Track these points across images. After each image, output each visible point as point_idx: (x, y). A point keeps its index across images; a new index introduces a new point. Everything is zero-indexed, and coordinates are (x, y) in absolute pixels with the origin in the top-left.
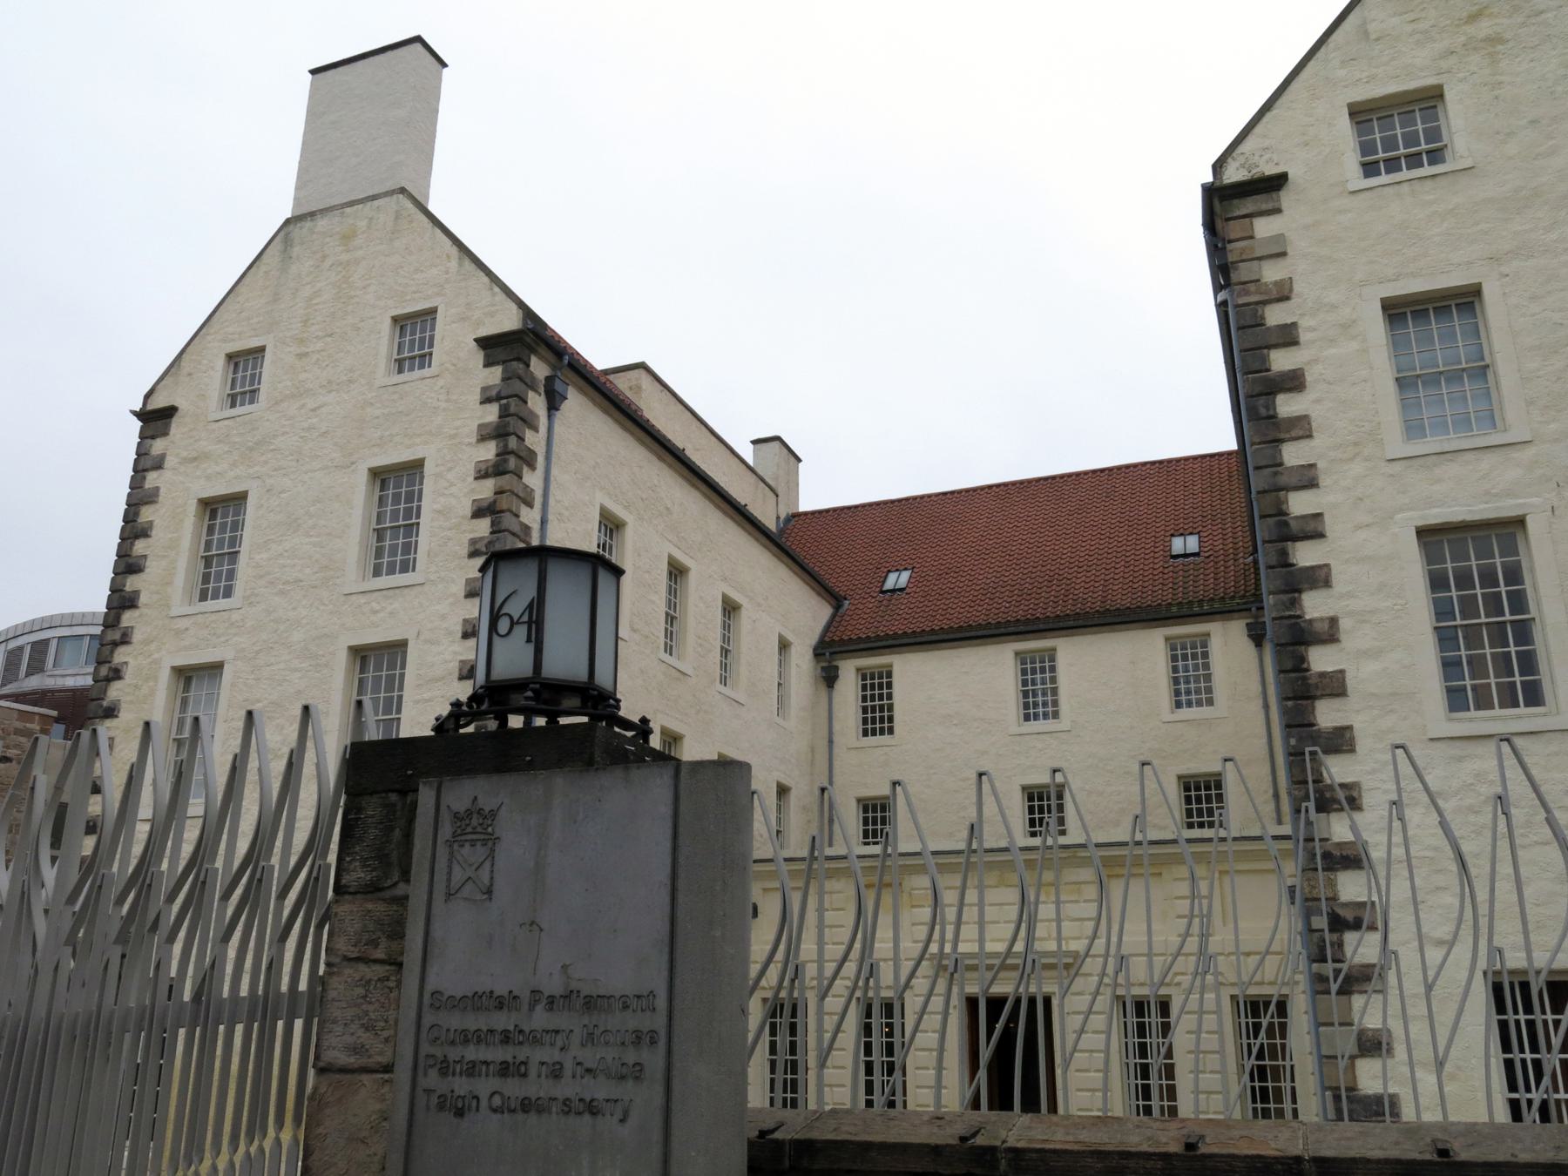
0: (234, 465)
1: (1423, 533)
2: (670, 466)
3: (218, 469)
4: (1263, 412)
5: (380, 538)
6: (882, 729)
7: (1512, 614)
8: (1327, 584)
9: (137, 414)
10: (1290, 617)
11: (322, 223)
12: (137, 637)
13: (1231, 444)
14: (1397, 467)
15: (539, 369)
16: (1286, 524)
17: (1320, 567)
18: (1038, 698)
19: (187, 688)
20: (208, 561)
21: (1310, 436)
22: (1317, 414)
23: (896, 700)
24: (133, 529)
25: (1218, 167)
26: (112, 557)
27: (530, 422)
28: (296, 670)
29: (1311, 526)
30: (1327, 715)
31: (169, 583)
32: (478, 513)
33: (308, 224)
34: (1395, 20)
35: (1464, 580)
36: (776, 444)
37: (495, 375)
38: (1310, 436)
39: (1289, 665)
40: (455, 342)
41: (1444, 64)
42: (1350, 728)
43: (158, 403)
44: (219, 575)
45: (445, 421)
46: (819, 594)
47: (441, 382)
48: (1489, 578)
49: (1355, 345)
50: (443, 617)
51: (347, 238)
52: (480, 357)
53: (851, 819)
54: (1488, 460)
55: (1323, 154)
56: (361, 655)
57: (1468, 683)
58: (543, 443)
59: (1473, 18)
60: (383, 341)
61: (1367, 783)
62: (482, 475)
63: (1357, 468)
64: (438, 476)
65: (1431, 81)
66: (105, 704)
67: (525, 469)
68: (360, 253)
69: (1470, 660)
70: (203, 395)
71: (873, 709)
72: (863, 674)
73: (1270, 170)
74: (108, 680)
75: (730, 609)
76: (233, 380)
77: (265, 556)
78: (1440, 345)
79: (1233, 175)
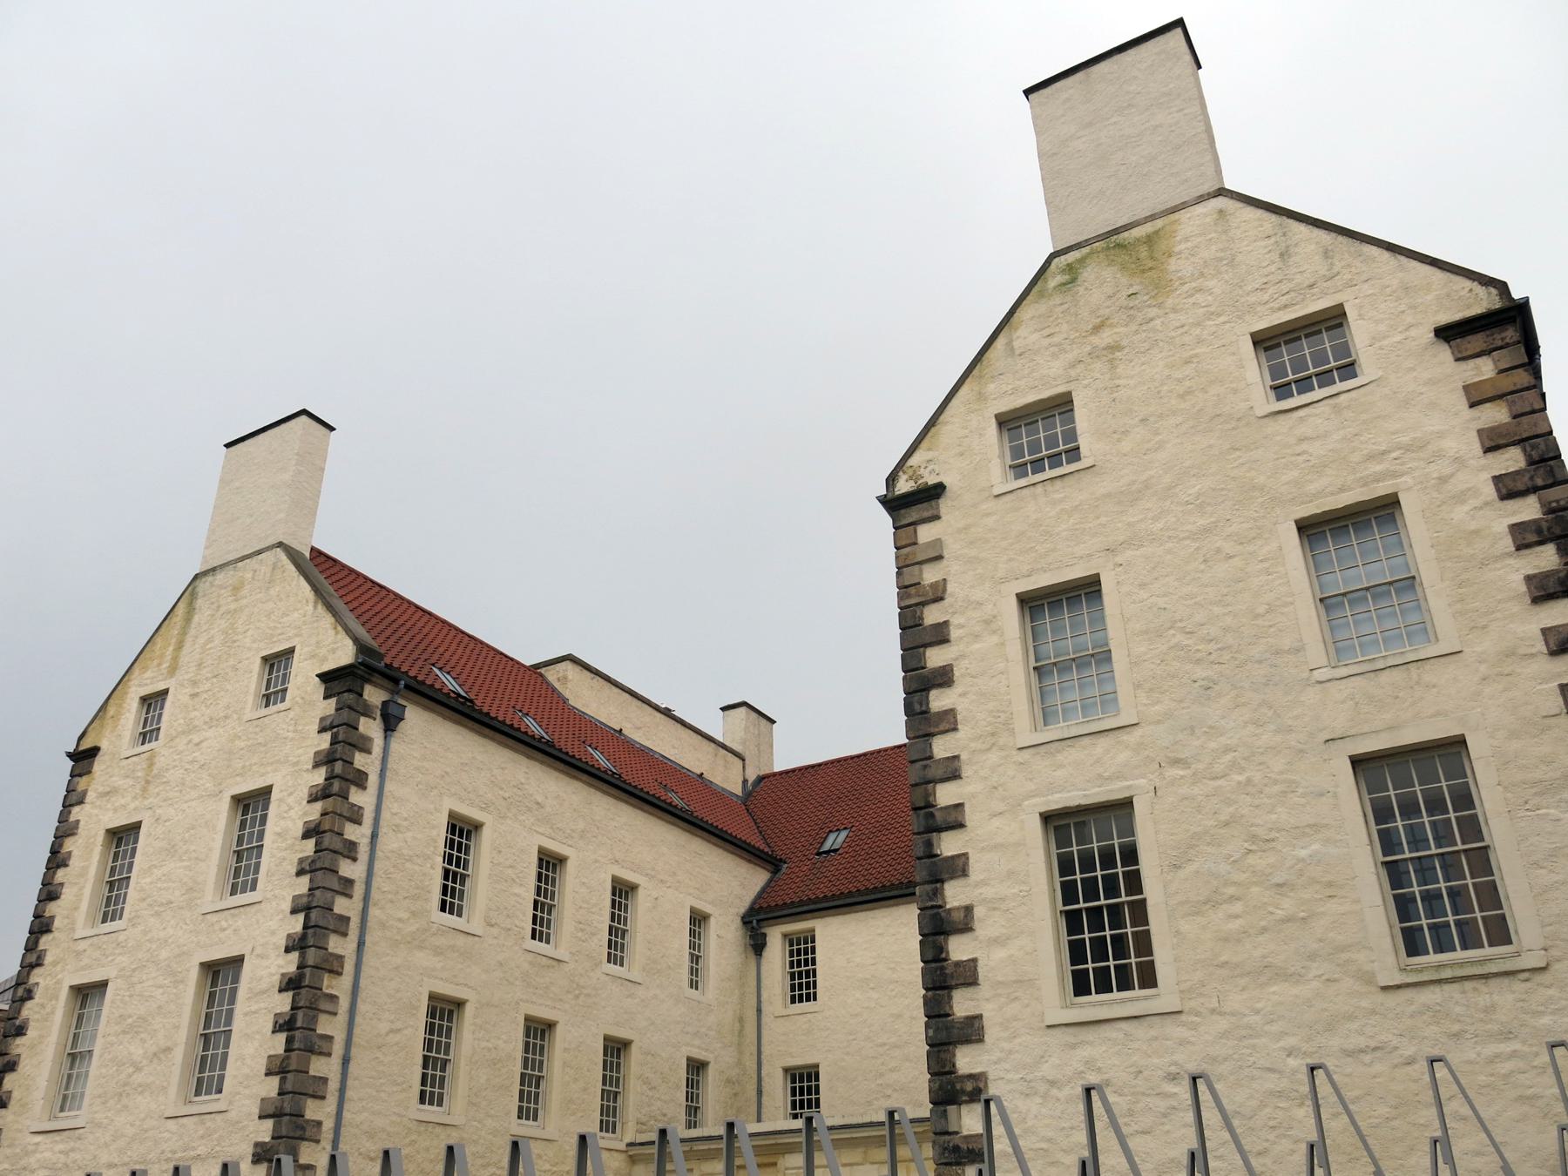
0: (135, 798)
1: (1047, 818)
2: (542, 763)
3: (123, 802)
4: (917, 708)
5: (239, 860)
6: (808, 995)
7: (1464, 843)
8: (964, 873)
9: (70, 755)
10: (933, 907)
11: (220, 577)
12: (48, 959)
13: (902, 739)
14: (1026, 754)
16: (932, 815)
17: (959, 856)
19: (83, 1006)
20: (239, 854)
21: (955, 729)
23: (818, 967)
25: (891, 480)
26: (37, 886)
27: (364, 746)
28: (160, 987)
29: (951, 819)
31: (76, 909)
32: (306, 835)
33: (210, 578)
34: (1036, 336)
35: (1409, 809)
36: (743, 710)
38: (955, 729)
39: (930, 957)
41: (1073, 373)
42: (980, 1017)
43: (86, 745)
44: (248, 867)
46: (749, 861)
47: (291, 714)
48: (1435, 805)
49: (995, 639)
50: (273, 933)
51: (236, 589)
52: (321, 689)
53: (778, 1092)
54: (1103, 743)
57: (1451, 918)
58: (378, 764)
59: (1097, 329)
60: (252, 678)
62: (313, 799)
63: (993, 757)
64: (281, 800)
65: (1061, 389)
66: (17, 1022)
67: (353, 789)
68: (244, 602)
69: (1450, 890)
70: (972, 461)
71: (800, 973)
72: (790, 939)
73: (932, 480)
74: (23, 1000)
76: (269, 681)
77: (148, 880)
78: (1360, 563)
79: (904, 486)
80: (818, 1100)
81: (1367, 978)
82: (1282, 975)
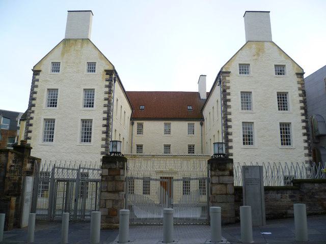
0: (55, 83)
18: (168, 132)
22: (232, 105)
25: (222, 69)
40: (100, 68)
43: (36, 69)
45: (98, 83)
50: (99, 116)
53: (135, 148)
56: (165, 146)
70: (47, 68)
71: (284, 136)
73: (229, 71)
75: (125, 112)
79: (224, 70)
80: (52, 139)
81: (278, 147)
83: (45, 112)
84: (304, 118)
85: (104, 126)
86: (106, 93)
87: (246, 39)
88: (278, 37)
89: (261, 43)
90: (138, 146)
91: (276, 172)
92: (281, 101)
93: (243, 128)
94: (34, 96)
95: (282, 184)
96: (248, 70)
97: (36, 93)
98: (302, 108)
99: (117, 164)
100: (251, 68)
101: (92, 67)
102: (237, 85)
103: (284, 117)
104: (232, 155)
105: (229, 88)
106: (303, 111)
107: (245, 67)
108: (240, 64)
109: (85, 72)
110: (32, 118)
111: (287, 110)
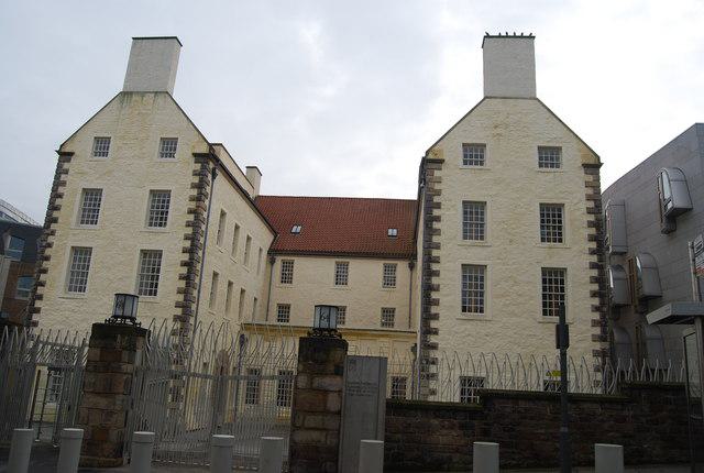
8: (438, 319)
15: (211, 165)
18: (341, 278)
24: (55, 195)
25: (427, 153)
30: (434, 310)
37: (198, 166)
40: (184, 152)
45: (179, 178)
53: (274, 311)
55: (454, 156)
56: (385, 311)
60: (156, 147)
61: (440, 328)
70: (84, 149)
71: (78, 273)
79: (431, 156)
82: (516, 315)
83: (74, 235)
84: (594, 259)
85: (184, 264)
86: (192, 199)
87: (125, 86)
88: (548, 89)
89: (511, 101)
90: (280, 306)
91: (496, 375)
92: (548, 221)
93: (464, 277)
94: (58, 201)
95: (457, 400)
96: (558, 159)
97: (60, 196)
98: (592, 238)
99: (118, 340)
100: (488, 154)
101: (169, 147)
102: (457, 187)
103: (555, 257)
104: (436, 333)
105: (438, 193)
106: (593, 245)
107: (476, 151)
108: (464, 145)
109: (157, 158)
110: (50, 245)
111: (560, 241)
